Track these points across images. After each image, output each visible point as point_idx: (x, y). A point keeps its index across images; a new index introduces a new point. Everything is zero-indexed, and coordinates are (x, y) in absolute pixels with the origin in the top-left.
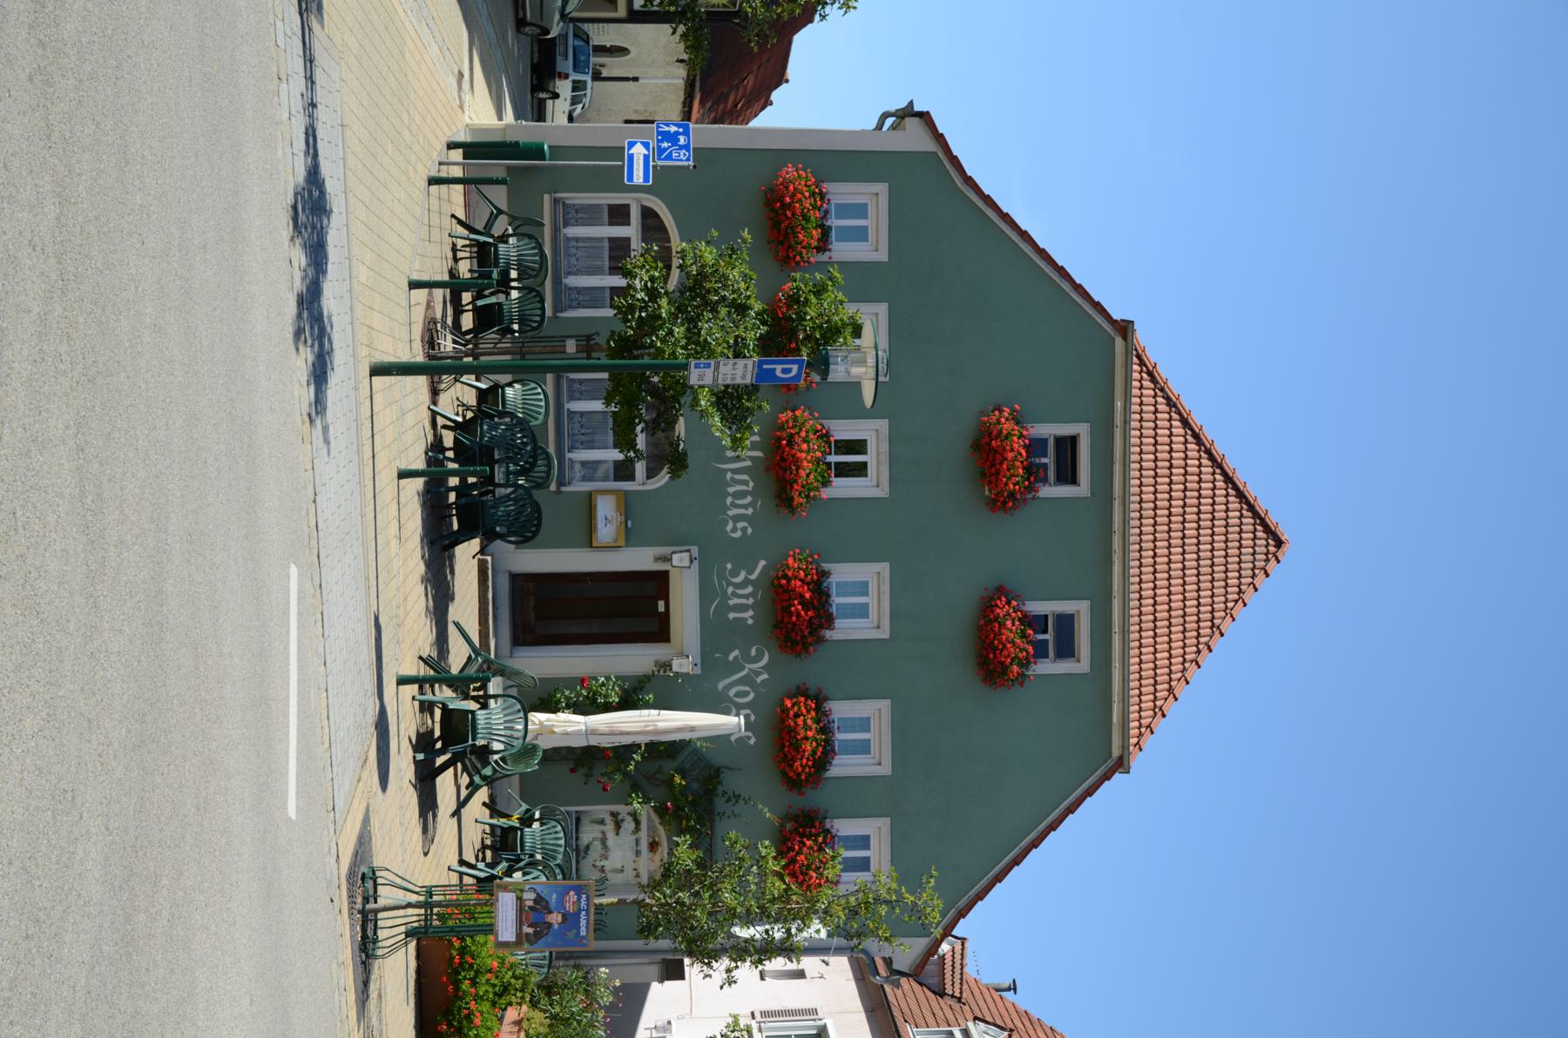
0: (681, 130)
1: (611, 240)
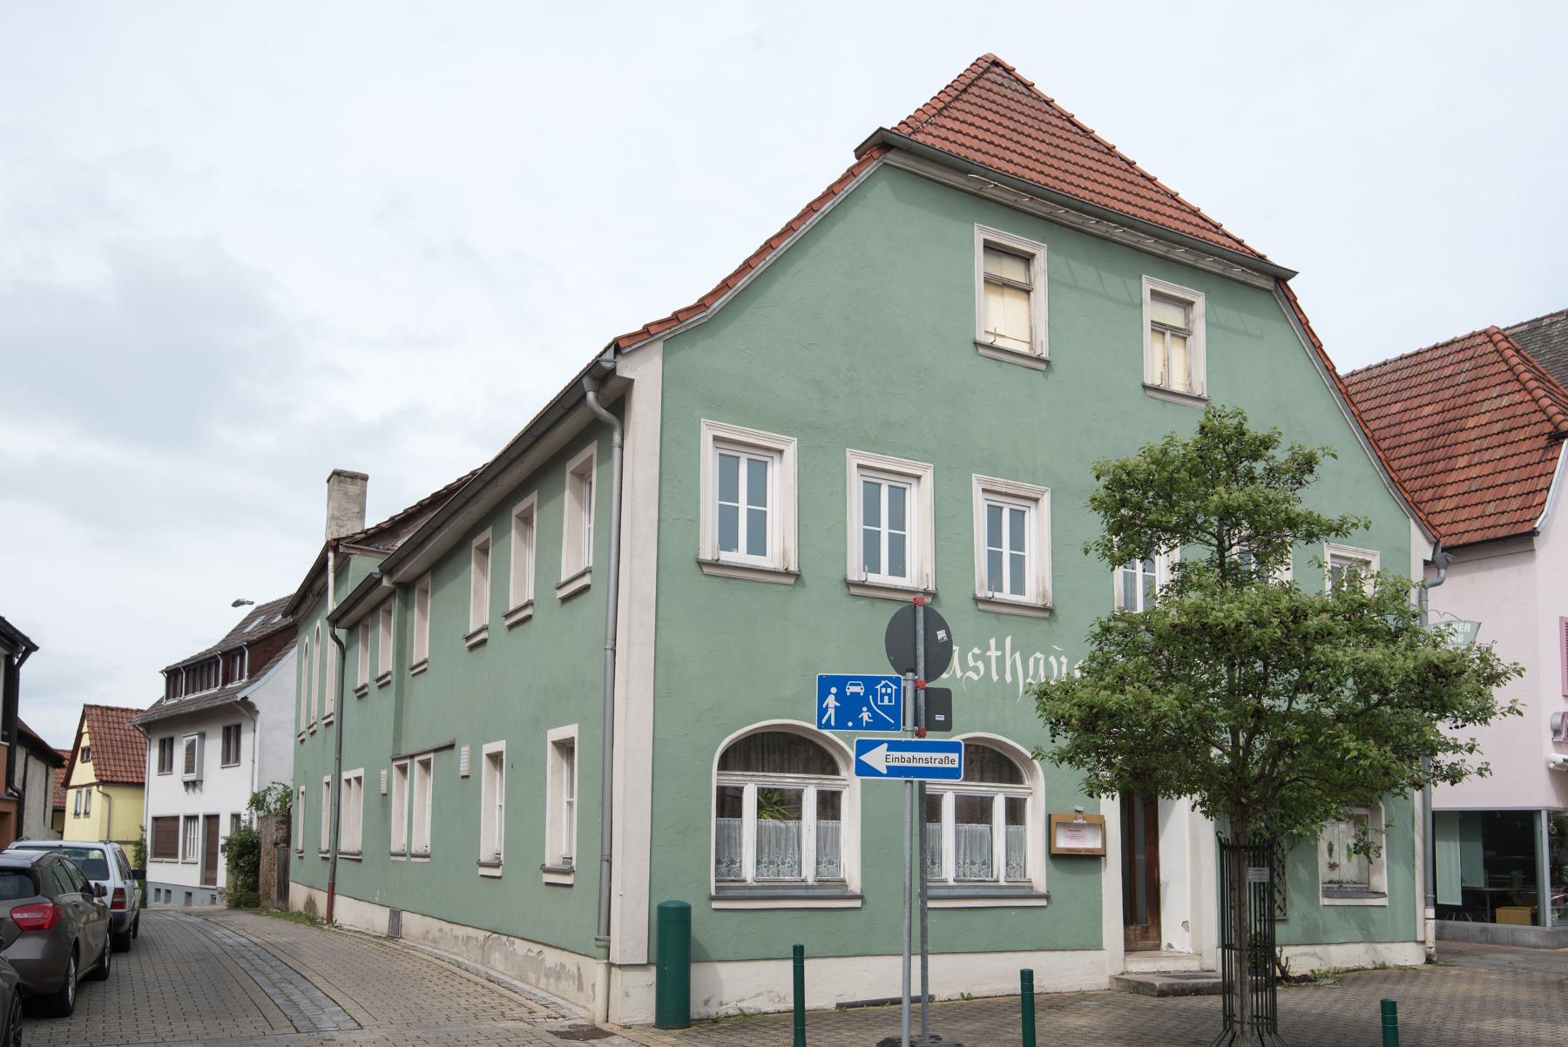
0: (834, 690)
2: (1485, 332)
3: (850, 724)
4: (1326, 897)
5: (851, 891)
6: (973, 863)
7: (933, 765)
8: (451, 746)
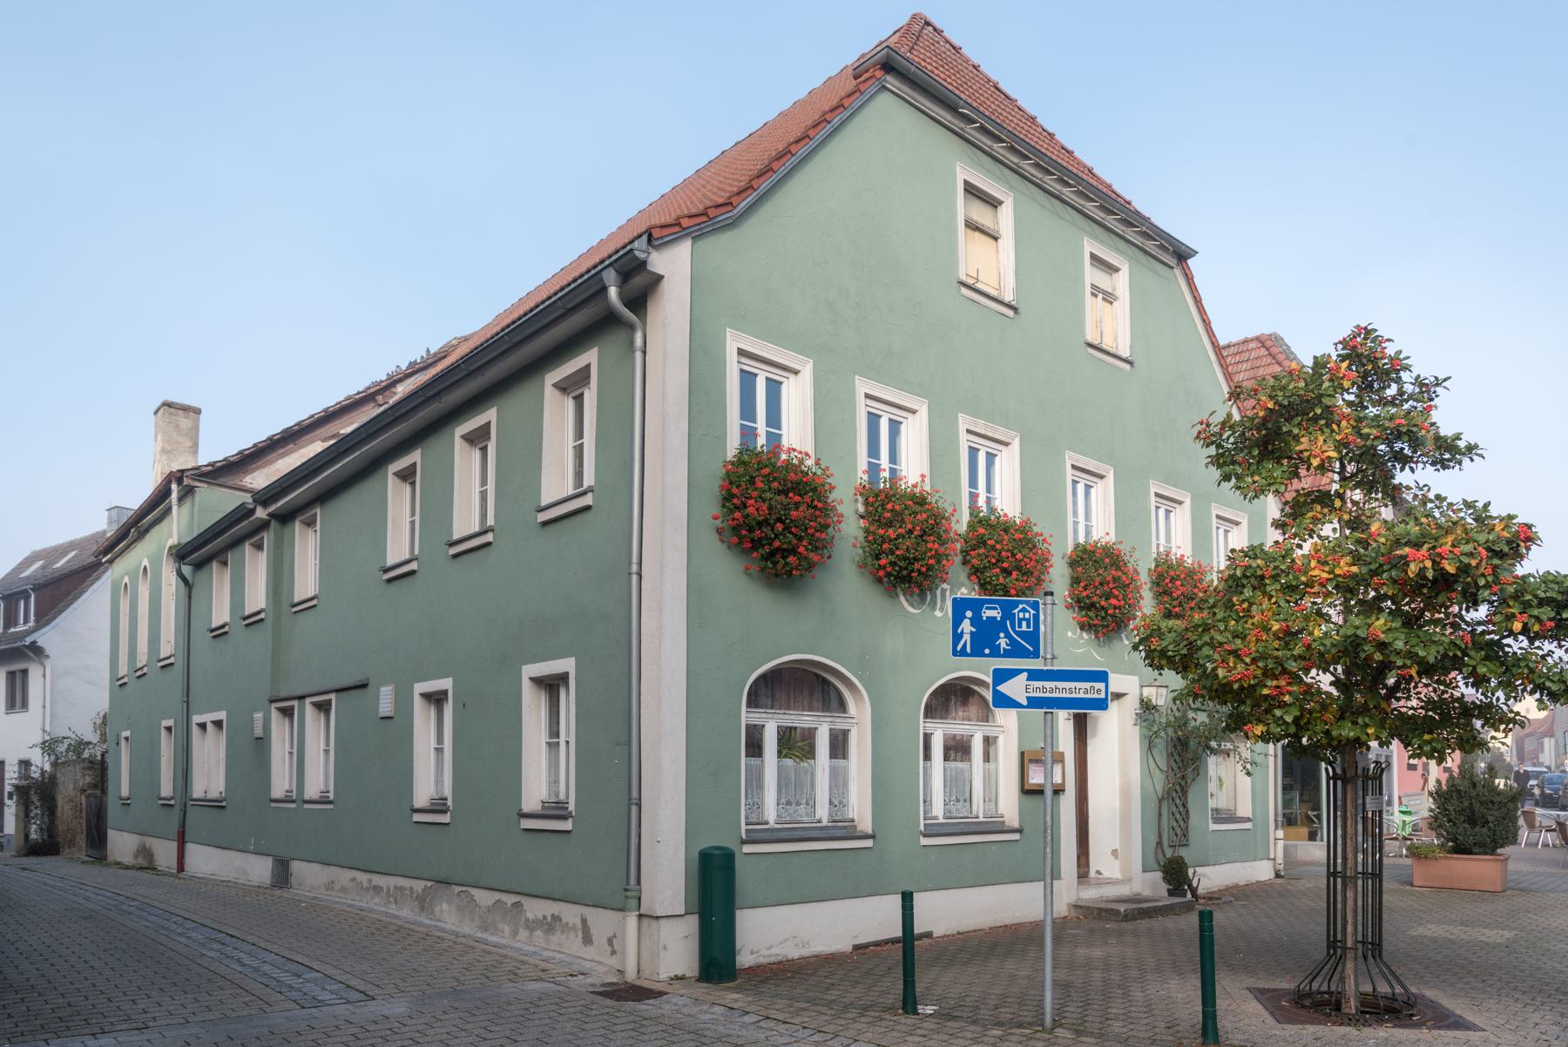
0: (969, 614)
1: (946, 758)
2: (1257, 339)
3: (987, 651)
4: (1215, 823)
5: (861, 832)
7: (1078, 696)
8: (364, 686)
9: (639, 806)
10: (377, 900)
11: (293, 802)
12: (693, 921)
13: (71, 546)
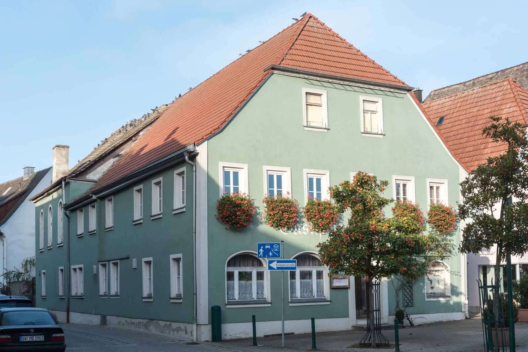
0: (262, 247)
3: (267, 256)
6: (307, 292)
8: (128, 258)
9: (196, 295)
10: (133, 327)
11: (107, 296)
12: (210, 326)
13: (8, 185)
